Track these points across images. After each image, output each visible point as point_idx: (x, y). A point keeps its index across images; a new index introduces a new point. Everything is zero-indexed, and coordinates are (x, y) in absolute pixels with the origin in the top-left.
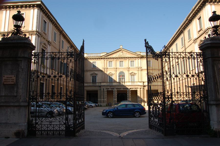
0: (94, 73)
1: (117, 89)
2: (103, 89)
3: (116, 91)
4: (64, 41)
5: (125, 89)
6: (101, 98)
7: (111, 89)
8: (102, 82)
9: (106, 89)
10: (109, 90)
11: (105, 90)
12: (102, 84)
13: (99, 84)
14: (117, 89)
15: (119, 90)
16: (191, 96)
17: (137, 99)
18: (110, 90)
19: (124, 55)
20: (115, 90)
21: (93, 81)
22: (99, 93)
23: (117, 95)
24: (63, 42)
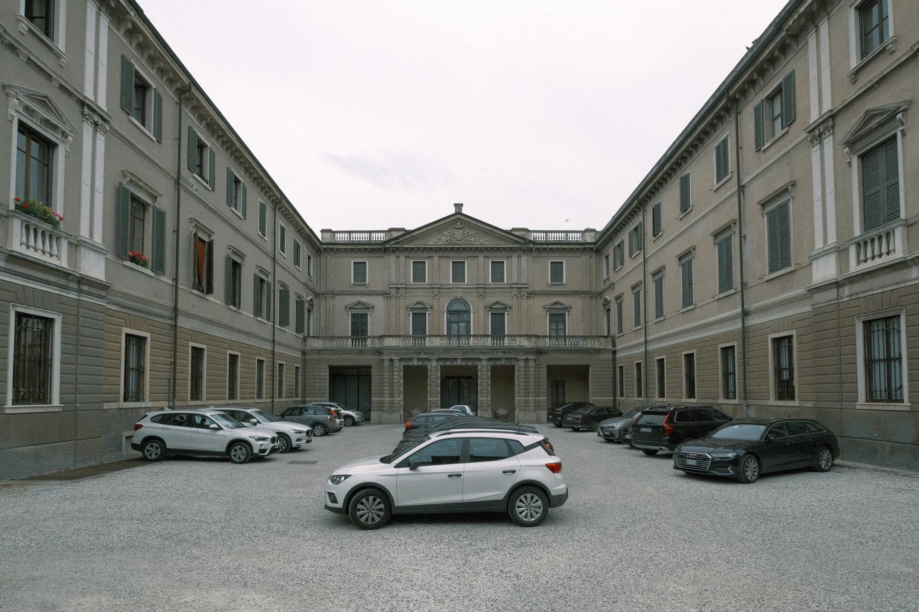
0: (359, 303)
1: (439, 360)
2: (391, 360)
3: (439, 368)
4: (300, 244)
5: (470, 363)
6: (381, 395)
7: (419, 359)
8: (386, 334)
9: (489, 360)
10: (411, 363)
11: (397, 364)
12: (389, 342)
13: (377, 344)
14: (439, 360)
15: (448, 363)
16: (533, 369)
17: (514, 398)
18: (415, 363)
19: (468, 238)
20: (434, 363)
21: (354, 332)
22: (374, 373)
23: (439, 382)
24: (283, 230)
